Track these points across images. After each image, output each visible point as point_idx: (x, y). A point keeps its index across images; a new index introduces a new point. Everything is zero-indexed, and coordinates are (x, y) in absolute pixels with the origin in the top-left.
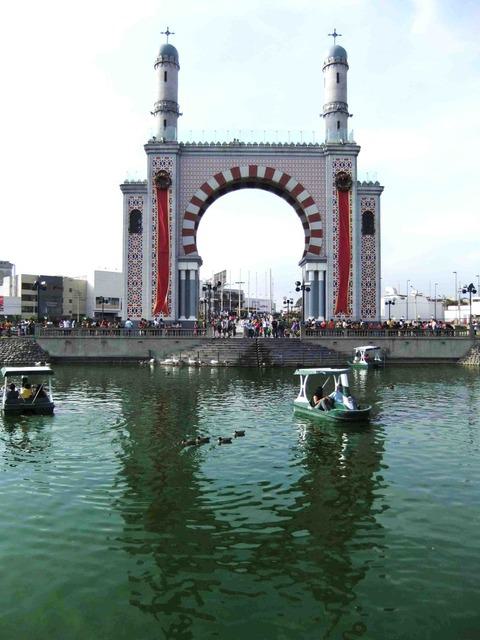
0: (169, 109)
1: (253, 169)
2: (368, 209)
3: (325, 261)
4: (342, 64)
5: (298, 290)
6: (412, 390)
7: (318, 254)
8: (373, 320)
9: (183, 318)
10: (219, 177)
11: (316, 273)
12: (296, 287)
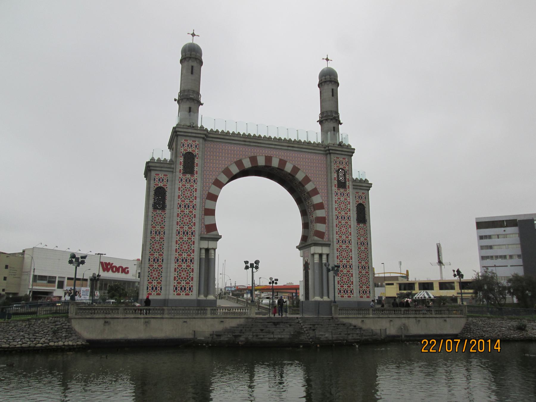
0: (190, 98)
1: (268, 159)
2: (161, 185)
3: (328, 245)
4: (331, 81)
5: (247, 268)
6: (263, 370)
7: (323, 238)
8: (159, 297)
9: (202, 297)
10: (239, 163)
11: (321, 255)
12: (244, 265)
